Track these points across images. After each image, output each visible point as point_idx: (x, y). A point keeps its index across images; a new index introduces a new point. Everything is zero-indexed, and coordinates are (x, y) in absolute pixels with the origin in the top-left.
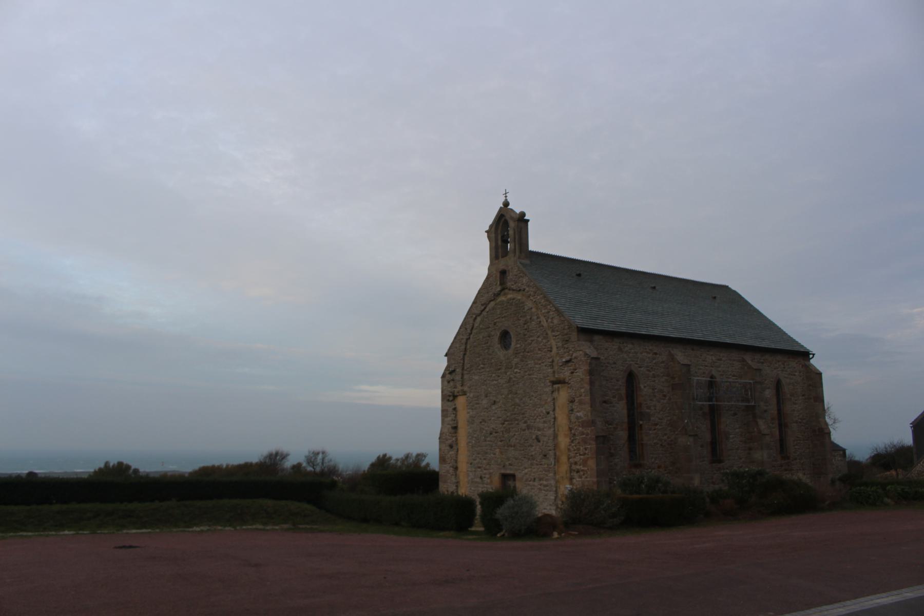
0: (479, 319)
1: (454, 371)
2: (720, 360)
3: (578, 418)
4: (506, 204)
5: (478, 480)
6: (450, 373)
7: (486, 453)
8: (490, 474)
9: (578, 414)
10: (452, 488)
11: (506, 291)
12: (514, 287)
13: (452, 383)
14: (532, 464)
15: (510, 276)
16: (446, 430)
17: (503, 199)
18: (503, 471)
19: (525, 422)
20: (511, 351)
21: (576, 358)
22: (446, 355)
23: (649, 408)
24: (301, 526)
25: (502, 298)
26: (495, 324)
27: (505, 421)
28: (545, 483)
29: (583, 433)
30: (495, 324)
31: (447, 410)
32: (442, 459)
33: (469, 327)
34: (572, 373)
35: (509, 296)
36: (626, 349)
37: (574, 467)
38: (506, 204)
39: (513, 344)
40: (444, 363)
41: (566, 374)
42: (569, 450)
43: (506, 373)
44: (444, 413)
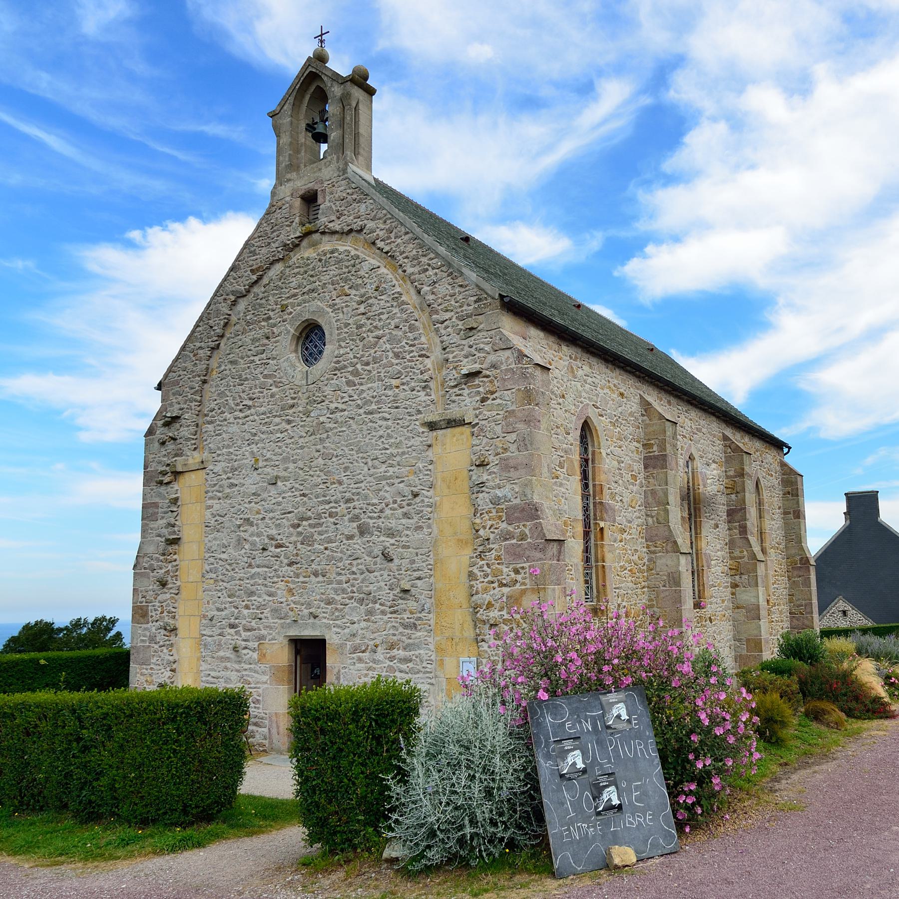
0: (242, 305)
1: (175, 419)
2: (699, 430)
3: (496, 501)
4: (320, 58)
5: (229, 654)
6: (167, 424)
7: (252, 594)
8: (261, 638)
9: (499, 493)
10: (164, 676)
11: (316, 236)
12: (336, 226)
13: (170, 446)
14: (370, 613)
15: (325, 203)
16: (150, 549)
17: (308, 50)
18: (294, 632)
19: (356, 518)
20: (323, 364)
21: (494, 366)
22: (159, 387)
23: (613, 496)
24: (298, 658)
25: (307, 252)
26: (284, 308)
27: (302, 519)
28: (401, 653)
29: (507, 536)
30: (284, 308)
31: (156, 505)
32: (140, 613)
33: (217, 323)
34: (483, 400)
35: (328, 247)
36: (580, 373)
37: (482, 614)
38: (320, 58)
39: (328, 349)
40: (33, 622)
41: (466, 404)
42: (471, 575)
43: (307, 414)
44: (149, 511)
